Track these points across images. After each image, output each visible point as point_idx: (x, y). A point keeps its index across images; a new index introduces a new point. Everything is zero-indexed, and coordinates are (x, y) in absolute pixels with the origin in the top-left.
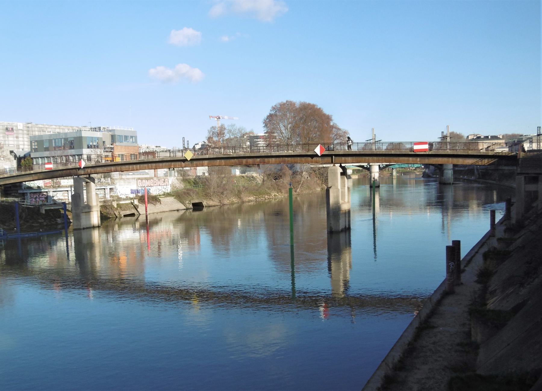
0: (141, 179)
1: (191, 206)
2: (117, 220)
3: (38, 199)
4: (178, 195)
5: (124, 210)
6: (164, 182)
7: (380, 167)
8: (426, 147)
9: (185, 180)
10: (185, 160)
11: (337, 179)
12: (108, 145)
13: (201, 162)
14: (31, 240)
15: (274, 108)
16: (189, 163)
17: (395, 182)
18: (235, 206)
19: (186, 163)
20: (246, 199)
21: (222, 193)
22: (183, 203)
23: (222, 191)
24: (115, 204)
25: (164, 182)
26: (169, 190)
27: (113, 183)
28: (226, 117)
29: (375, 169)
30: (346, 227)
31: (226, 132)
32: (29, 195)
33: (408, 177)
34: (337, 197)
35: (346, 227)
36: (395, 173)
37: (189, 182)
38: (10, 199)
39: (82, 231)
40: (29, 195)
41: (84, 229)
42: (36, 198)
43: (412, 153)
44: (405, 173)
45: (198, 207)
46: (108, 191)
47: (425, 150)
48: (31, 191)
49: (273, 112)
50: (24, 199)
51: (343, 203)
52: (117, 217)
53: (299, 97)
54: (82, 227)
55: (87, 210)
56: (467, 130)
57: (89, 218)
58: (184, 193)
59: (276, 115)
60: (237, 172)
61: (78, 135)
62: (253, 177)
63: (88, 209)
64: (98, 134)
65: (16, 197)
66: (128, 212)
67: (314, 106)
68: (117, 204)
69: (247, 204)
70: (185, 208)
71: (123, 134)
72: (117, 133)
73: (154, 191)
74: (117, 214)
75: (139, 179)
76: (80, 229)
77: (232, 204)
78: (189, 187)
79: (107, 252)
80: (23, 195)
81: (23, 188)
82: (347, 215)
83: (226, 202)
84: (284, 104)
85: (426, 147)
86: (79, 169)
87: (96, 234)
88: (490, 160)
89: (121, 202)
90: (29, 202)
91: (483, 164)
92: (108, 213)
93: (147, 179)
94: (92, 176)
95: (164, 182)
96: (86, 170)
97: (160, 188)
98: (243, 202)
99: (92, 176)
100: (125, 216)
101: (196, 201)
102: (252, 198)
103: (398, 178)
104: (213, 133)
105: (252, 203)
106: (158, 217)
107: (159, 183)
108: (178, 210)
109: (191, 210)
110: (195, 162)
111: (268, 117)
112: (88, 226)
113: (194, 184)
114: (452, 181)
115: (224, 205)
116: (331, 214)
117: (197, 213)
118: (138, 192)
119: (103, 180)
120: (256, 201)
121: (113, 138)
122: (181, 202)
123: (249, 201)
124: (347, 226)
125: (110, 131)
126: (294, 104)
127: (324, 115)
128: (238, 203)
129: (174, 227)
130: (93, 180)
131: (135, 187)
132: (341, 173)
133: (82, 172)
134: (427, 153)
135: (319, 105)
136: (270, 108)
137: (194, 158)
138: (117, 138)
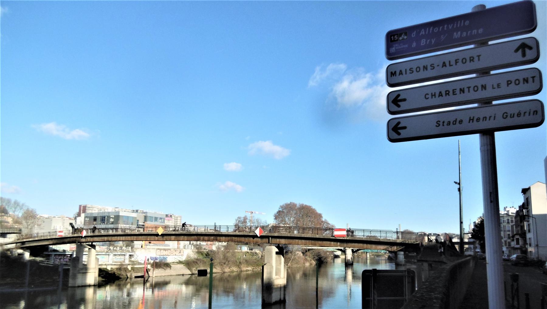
0: (161, 250)
1: (197, 272)
2: (128, 280)
3: (62, 260)
4: (188, 264)
5: (137, 272)
6: (182, 251)
7: (352, 250)
8: (345, 233)
9: (199, 253)
10: (157, 235)
11: (271, 257)
12: (141, 223)
13: (169, 237)
14: (45, 293)
15: (282, 207)
16: (161, 237)
17: (368, 261)
18: (235, 273)
19: (159, 237)
20: (244, 269)
21: (225, 263)
22: (189, 269)
23: (226, 261)
24: (129, 268)
25: (180, 252)
26: (183, 259)
27: (133, 251)
28: (257, 213)
29: (349, 252)
30: (280, 299)
31: (248, 221)
32: (53, 256)
33: (380, 258)
34: (271, 273)
35: (280, 299)
36: (368, 256)
37: (202, 254)
38: (38, 259)
39: (76, 289)
40: (53, 256)
41: (79, 287)
42: (60, 259)
43: (333, 238)
44: (378, 256)
45: (202, 273)
46: (127, 257)
47: (343, 236)
48: (56, 253)
49: (280, 209)
50: (49, 259)
51: (277, 279)
52: (128, 278)
53: (299, 201)
54: (77, 285)
55: (84, 271)
56: (417, 229)
57: (85, 278)
58: (194, 262)
59: (283, 212)
60: (245, 249)
61: (117, 214)
62: (256, 253)
63: (85, 269)
64: (134, 215)
65: (43, 257)
66: (139, 274)
67: (310, 207)
68: (132, 268)
69: (245, 272)
70: (190, 273)
71: (154, 216)
72: (148, 215)
73: (169, 260)
74: (129, 275)
75: (158, 249)
76: (74, 287)
77: (232, 272)
78: (201, 257)
79: (121, 304)
80: (48, 257)
81: (49, 250)
82: (282, 289)
83: (227, 270)
84: (289, 205)
85: (345, 233)
86: (82, 237)
87: (90, 292)
88: (398, 247)
89: (135, 266)
90: (52, 261)
91: (393, 250)
92: (120, 274)
93: (165, 250)
94: (94, 243)
95: (180, 252)
96: (87, 238)
97: (176, 257)
98: (241, 271)
99: (94, 243)
100: (136, 277)
101: (202, 268)
102: (250, 268)
103: (371, 259)
104: (239, 221)
105: (250, 272)
106: (167, 279)
107: (175, 253)
108: (183, 275)
109: (197, 275)
110: (165, 237)
111: (278, 212)
112: (83, 285)
113: (206, 255)
114: (403, 263)
115: (224, 272)
116: (264, 288)
117: (202, 278)
118: (156, 259)
119: (124, 248)
120: (253, 271)
121: (146, 218)
122: (188, 269)
123: (247, 271)
124: (282, 299)
125: (144, 213)
126: (296, 205)
127: (317, 213)
128: (237, 271)
129: (186, 287)
130: (94, 247)
131: (154, 256)
132: (277, 253)
133: (83, 240)
134: (346, 238)
135: (314, 207)
136: (279, 206)
137: (164, 233)
138: (148, 219)
